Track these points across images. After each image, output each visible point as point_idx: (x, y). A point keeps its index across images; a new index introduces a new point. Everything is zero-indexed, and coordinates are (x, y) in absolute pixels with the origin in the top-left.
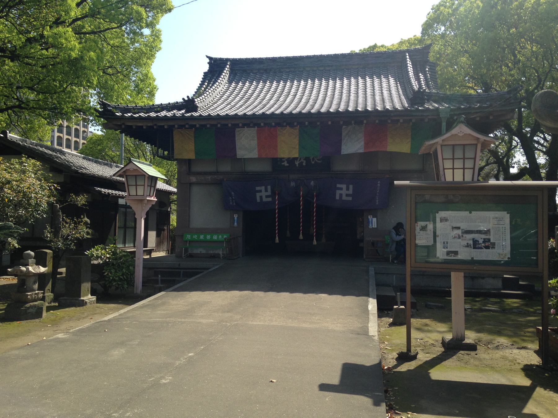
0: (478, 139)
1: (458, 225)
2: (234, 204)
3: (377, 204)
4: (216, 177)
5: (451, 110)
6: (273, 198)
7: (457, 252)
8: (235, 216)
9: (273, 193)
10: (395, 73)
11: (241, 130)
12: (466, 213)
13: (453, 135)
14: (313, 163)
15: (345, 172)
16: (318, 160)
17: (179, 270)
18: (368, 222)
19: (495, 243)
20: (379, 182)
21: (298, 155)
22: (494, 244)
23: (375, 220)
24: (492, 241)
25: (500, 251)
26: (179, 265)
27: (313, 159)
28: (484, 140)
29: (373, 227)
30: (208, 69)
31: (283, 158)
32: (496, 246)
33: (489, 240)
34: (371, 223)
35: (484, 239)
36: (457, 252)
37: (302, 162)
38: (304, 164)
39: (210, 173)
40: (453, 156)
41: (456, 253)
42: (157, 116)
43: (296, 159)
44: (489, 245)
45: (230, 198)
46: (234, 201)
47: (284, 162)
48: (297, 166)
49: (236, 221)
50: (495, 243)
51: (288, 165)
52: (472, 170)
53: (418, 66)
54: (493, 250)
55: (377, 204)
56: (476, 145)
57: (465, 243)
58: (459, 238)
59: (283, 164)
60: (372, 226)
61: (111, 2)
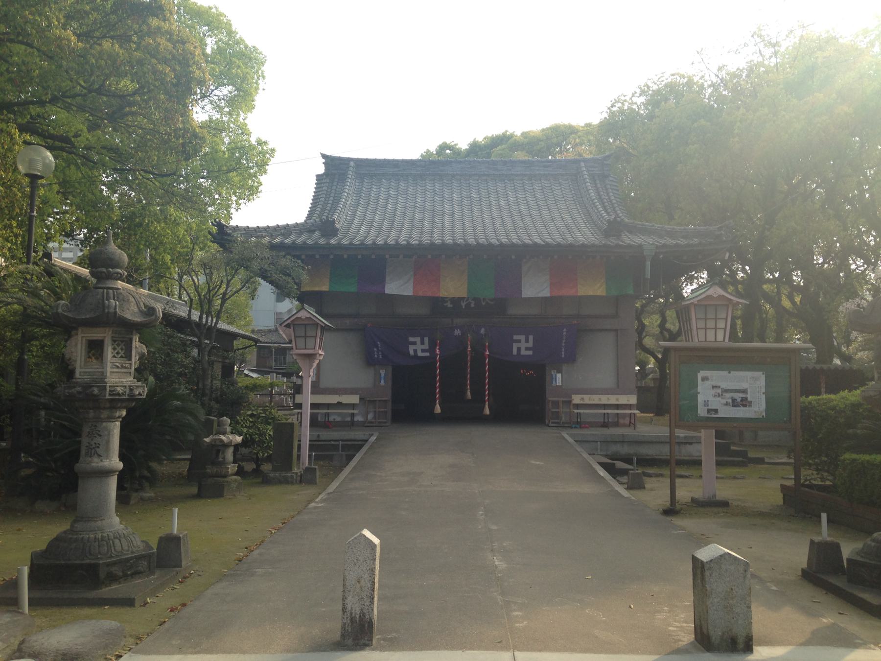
1: (718, 384)
2: (381, 357)
7: (717, 410)
9: (432, 345)
10: (575, 203)
12: (725, 373)
14: (484, 304)
17: (337, 443)
20: (565, 330)
22: (751, 402)
23: (559, 376)
24: (749, 399)
25: (756, 409)
26: (319, 436)
29: (558, 384)
30: (324, 168)
31: (447, 298)
33: (746, 399)
34: (554, 380)
35: (742, 398)
36: (717, 410)
37: (470, 303)
38: (472, 305)
40: (716, 316)
41: (716, 411)
43: (463, 298)
44: (745, 403)
45: (375, 349)
47: (447, 302)
48: (464, 307)
50: (751, 402)
51: (451, 306)
54: (750, 408)
55: (563, 356)
57: (724, 401)
58: (719, 396)
59: (445, 305)
61: (877, 259)
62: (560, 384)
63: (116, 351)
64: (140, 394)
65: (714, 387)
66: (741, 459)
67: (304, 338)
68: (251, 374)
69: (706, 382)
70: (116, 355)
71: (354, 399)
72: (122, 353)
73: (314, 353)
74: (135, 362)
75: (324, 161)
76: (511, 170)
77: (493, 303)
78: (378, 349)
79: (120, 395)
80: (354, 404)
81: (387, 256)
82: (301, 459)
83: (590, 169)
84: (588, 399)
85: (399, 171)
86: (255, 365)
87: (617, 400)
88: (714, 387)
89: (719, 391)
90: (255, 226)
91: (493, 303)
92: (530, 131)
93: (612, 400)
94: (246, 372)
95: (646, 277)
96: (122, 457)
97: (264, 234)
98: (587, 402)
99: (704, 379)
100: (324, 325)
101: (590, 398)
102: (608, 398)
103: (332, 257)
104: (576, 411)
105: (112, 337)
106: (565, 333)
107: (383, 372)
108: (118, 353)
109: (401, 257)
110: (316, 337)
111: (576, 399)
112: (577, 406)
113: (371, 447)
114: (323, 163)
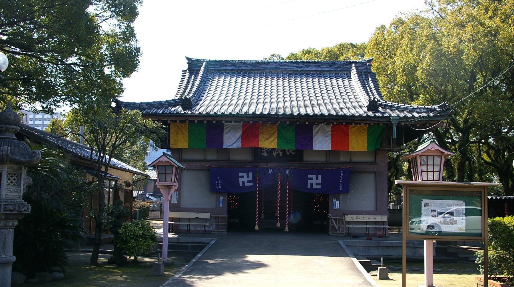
0: (443, 152)
2: (220, 187)
3: (341, 189)
4: (204, 164)
5: (399, 118)
6: (255, 184)
8: (220, 198)
9: (254, 181)
11: (228, 125)
13: (428, 150)
14: (288, 154)
15: (314, 162)
16: (292, 151)
18: (333, 204)
19: (456, 221)
20: (342, 172)
21: (276, 146)
23: (338, 202)
25: (460, 226)
27: (288, 151)
28: (447, 154)
32: (457, 223)
34: (335, 205)
37: (279, 153)
38: (281, 155)
39: (200, 161)
42: (185, 113)
43: (273, 150)
45: (216, 182)
46: (220, 185)
47: (264, 152)
48: (275, 156)
49: (221, 203)
50: (456, 221)
51: (267, 155)
52: (439, 173)
53: (363, 76)
56: (441, 156)
59: (263, 154)
60: (336, 207)
62: (339, 208)
63: (10, 181)
64: (25, 210)
65: (432, 211)
66: (119, 271)
67: (426, 172)
68: (150, 197)
69: (427, 207)
70: (10, 183)
71: (207, 216)
72: (14, 182)
73: (170, 184)
74: (24, 189)
75: (187, 61)
76: (308, 68)
77: (294, 153)
78: (218, 182)
79: (12, 211)
80: (206, 219)
81: (224, 122)
82: (163, 254)
83: (359, 68)
84: (355, 218)
85: (235, 68)
86: (153, 191)
87: (375, 218)
88: (432, 211)
89: (435, 213)
90: (140, 102)
91: (294, 153)
92: (342, 47)
93: (372, 218)
94: (147, 196)
95: (394, 137)
96: (15, 253)
97: (145, 107)
98: (355, 220)
99: (426, 205)
100: (177, 166)
101: (357, 217)
102: (369, 218)
103: (205, 122)
104: (348, 226)
105: (7, 171)
106: (342, 174)
107: (221, 198)
108: (11, 182)
109: (233, 122)
110: (172, 174)
111: (348, 218)
112: (349, 222)
113: (210, 248)
114: (187, 63)
